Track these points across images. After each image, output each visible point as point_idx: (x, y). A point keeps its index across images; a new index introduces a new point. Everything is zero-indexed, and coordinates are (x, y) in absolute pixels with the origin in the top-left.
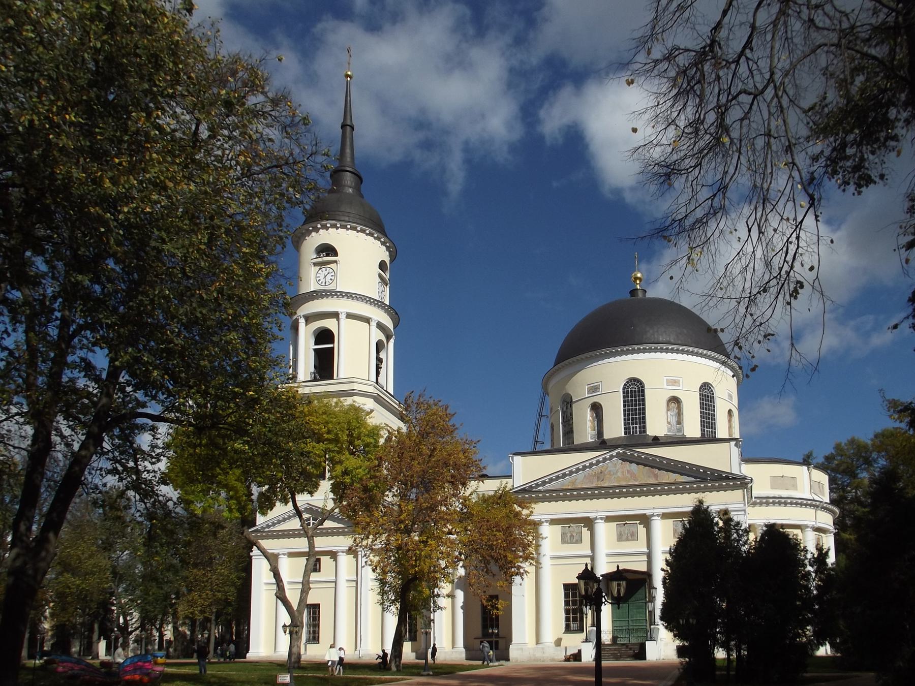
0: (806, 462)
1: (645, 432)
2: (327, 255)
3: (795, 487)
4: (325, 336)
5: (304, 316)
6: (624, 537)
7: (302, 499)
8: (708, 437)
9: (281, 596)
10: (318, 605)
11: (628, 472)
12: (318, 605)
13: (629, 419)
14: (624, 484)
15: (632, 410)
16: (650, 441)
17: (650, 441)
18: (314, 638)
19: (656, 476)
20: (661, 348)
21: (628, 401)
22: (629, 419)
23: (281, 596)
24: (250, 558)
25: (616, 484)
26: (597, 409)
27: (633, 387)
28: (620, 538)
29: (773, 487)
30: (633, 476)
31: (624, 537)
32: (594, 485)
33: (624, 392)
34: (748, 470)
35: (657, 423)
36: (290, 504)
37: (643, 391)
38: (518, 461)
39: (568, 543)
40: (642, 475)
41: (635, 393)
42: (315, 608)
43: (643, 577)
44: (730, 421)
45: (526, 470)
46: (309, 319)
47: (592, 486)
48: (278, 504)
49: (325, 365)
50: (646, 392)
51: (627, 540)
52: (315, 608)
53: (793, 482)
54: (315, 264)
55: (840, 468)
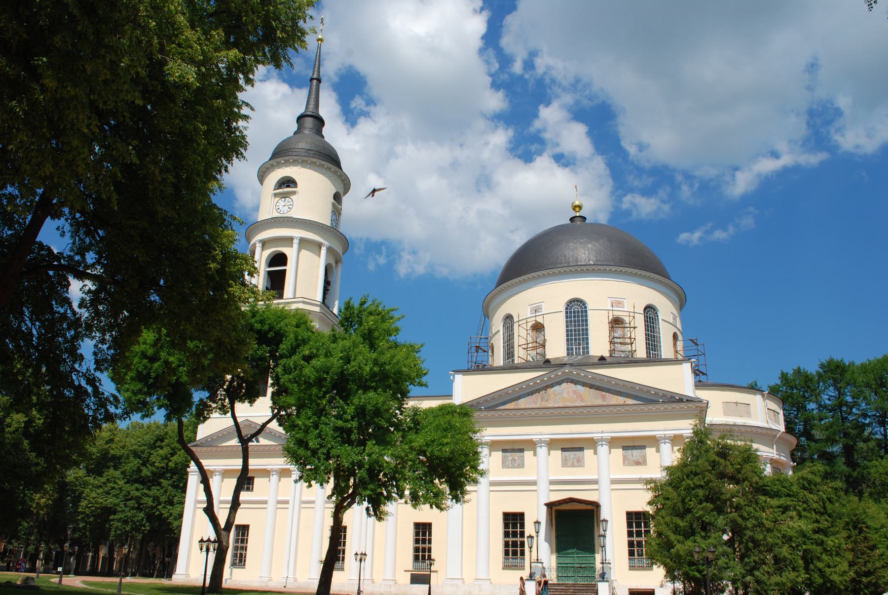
0: (753, 388)
1: (588, 353)
2: (288, 186)
3: (748, 414)
4: (279, 259)
5: (260, 241)
6: (570, 463)
7: (243, 410)
8: (653, 358)
9: (209, 511)
10: (248, 526)
11: (574, 392)
12: (248, 526)
13: (572, 340)
14: (570, 404)
15: (575, 330)
16: (596, 361)
17: (596, 361)
18: (240, 560)
19: (604, 397)
20: (605, 270)
21: (571, 321)
22: (572, 340)
23: (209, 511)
24: (187, 473)
25: (561, 405)
26: (538, 328)
27: (576, 308)
28: (565, 464)
29: (726, 413)
30: (580, 397)
31: (570, 463)
32: (537, 406)
33: (567, 313)
34: (703, 394)
35: (599, 343)
36: (229, 415)
37: (586, 312)
38: (459, 379)
39: (508, 467)
40: (591, 397)
41: (576, 312)
42: (244, 530)
43: (590, 507)
44: (675, 345)
45: (467, 389)
46: (265, 243)
47: (535, 406)
48: (215, 415)
49: (277, 281)
50: (589, 313)
51: (573, 466)
52: (244, 530)
53: (729, 407)
54: (276, 195)
55: (792, 393)
